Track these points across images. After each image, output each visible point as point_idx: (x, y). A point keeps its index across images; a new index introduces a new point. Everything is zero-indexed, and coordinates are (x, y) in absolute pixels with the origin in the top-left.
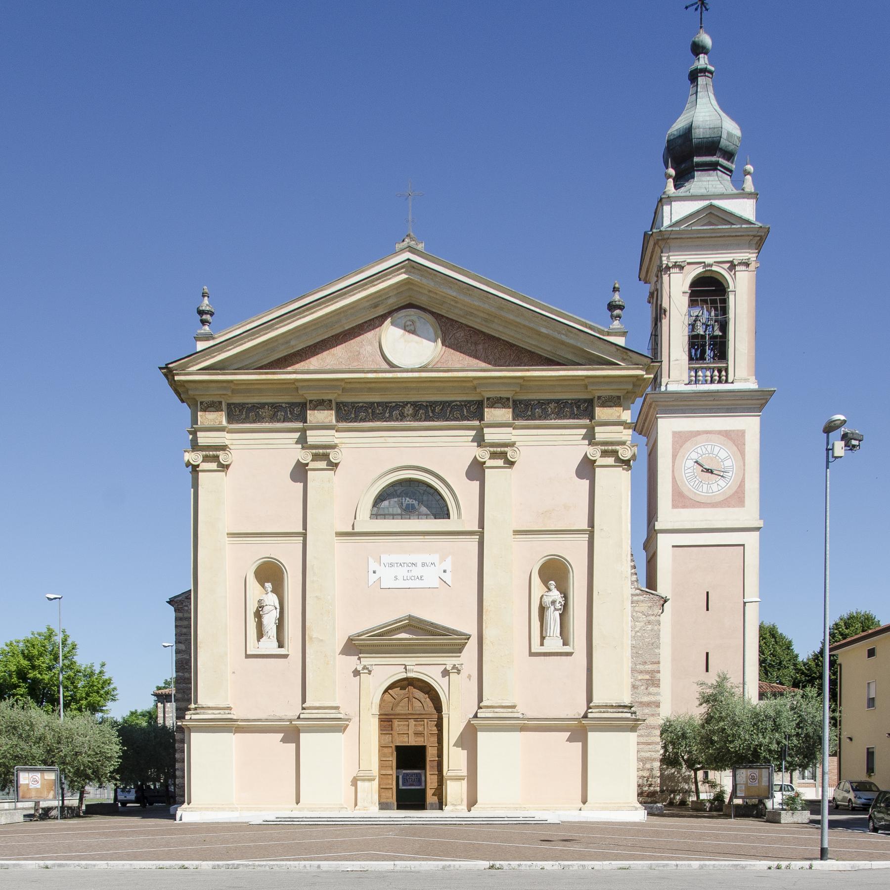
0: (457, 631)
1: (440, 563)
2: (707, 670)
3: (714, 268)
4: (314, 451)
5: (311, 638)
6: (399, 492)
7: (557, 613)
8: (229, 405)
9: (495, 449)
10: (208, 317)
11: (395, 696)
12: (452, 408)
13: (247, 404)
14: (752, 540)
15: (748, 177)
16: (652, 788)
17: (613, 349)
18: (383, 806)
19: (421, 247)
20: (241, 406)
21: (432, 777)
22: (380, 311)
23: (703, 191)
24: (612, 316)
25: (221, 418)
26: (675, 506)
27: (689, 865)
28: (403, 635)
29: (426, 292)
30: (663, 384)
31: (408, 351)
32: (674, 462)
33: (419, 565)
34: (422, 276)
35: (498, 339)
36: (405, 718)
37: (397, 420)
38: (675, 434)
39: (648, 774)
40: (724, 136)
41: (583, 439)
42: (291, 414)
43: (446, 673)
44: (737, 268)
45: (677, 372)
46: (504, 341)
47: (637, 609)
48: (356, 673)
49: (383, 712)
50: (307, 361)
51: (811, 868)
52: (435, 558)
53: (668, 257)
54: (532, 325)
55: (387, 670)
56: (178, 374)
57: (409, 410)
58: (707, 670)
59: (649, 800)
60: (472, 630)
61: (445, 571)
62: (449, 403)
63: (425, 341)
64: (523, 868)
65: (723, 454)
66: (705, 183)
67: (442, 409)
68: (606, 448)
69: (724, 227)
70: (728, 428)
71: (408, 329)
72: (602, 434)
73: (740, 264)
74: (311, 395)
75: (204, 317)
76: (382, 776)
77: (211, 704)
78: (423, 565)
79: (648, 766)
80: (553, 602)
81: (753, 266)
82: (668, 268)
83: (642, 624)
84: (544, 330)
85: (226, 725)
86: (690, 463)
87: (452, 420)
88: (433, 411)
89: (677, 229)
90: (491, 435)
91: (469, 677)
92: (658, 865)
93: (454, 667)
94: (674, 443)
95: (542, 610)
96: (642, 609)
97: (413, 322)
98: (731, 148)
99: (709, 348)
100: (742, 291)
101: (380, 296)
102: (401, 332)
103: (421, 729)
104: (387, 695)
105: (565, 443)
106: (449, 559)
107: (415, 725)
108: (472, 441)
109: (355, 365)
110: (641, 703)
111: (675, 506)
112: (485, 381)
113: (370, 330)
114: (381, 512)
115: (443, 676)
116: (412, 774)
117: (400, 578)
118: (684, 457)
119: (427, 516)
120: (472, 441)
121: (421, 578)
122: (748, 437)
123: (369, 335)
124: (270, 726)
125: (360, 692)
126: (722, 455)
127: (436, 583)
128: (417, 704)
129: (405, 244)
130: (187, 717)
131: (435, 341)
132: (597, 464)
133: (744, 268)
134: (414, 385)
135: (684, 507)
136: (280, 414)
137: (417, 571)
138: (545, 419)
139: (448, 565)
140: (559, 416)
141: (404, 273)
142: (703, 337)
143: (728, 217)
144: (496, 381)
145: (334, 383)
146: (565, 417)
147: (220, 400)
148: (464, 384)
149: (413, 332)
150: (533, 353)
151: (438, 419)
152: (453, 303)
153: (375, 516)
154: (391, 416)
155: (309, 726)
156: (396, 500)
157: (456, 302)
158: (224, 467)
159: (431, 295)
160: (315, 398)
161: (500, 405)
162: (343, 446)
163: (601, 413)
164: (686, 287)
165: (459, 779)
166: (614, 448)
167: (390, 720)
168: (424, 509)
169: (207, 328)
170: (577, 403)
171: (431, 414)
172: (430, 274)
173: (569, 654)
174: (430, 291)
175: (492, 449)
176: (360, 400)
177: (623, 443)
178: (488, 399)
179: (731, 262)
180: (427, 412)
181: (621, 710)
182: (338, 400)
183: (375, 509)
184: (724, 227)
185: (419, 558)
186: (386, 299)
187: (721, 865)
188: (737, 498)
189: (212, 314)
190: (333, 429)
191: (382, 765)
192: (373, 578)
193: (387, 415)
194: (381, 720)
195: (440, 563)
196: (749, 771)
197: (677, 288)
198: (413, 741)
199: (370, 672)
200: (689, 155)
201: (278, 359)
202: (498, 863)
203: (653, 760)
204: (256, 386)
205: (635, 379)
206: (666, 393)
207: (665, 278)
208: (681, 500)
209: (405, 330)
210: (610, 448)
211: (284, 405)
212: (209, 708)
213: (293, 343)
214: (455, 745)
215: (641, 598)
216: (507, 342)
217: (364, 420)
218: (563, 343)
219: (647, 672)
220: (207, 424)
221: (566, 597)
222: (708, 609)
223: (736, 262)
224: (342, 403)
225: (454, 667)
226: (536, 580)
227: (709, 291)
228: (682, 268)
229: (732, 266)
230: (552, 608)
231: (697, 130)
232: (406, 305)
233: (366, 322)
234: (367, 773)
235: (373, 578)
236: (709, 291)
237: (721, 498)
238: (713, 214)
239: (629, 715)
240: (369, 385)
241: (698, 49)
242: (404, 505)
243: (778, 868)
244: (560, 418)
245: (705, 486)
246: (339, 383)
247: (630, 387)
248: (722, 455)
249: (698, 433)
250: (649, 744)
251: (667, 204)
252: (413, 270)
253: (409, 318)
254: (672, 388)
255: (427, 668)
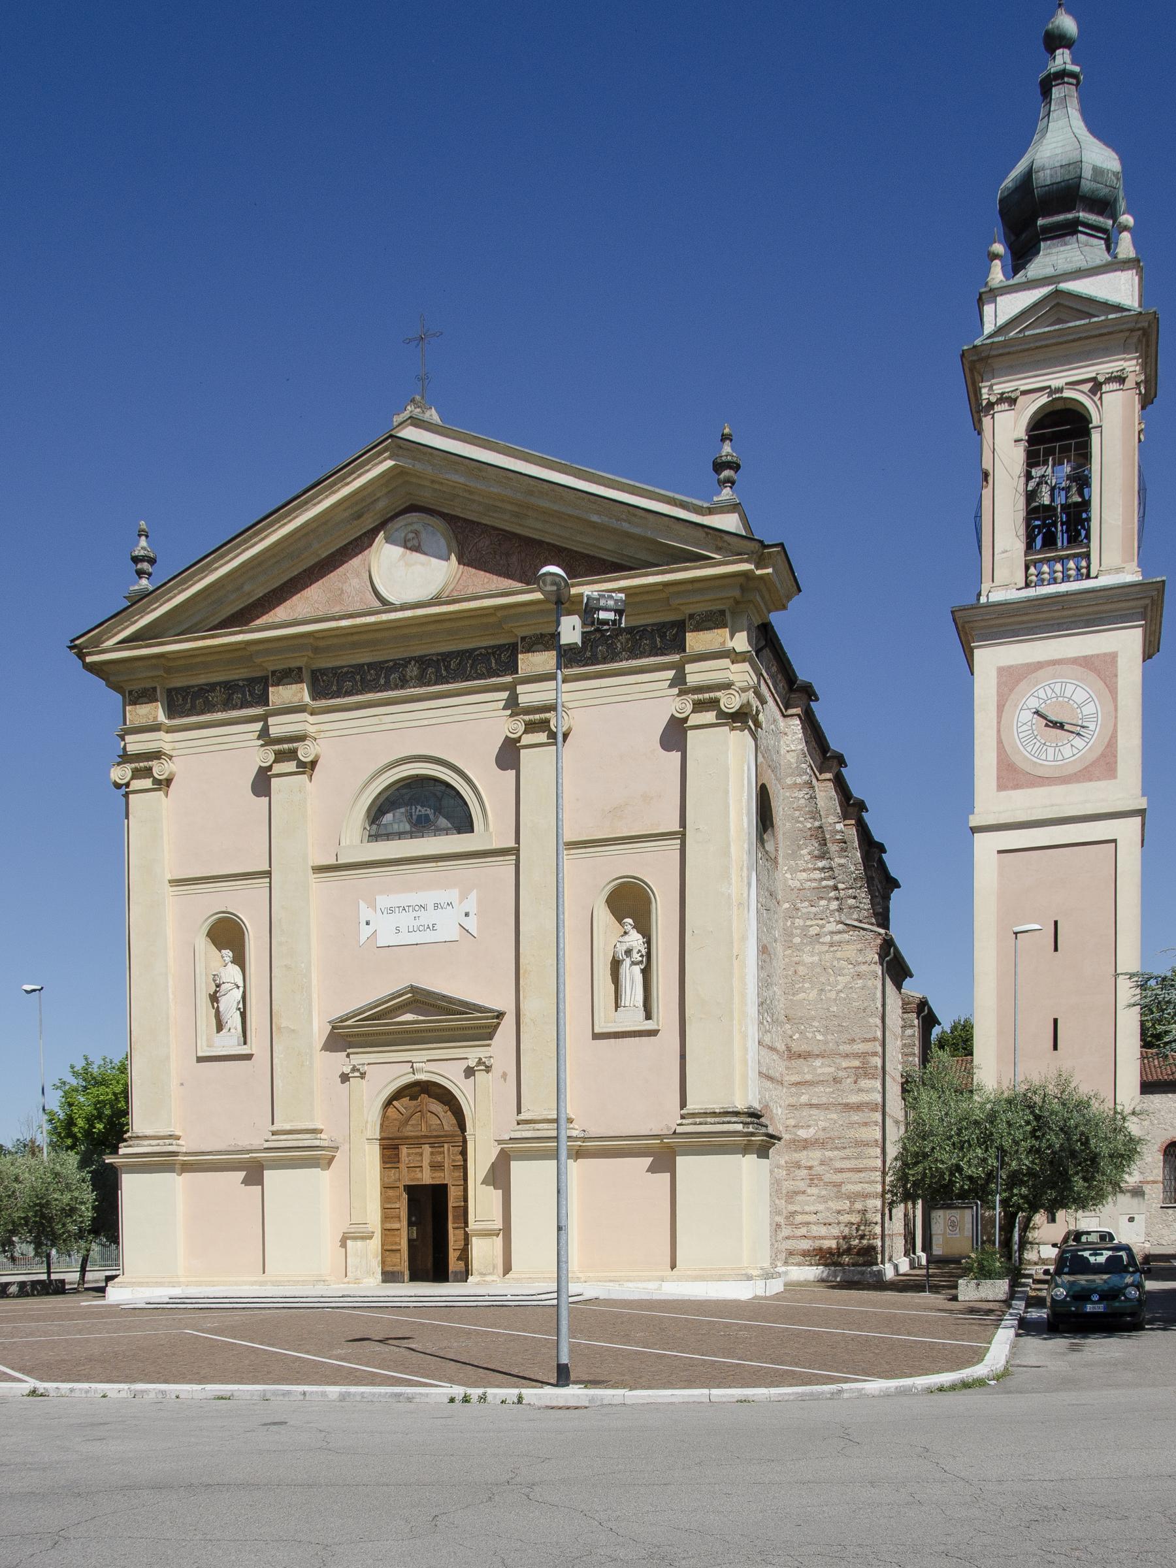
0: (480, 1007)
1: (460, 903)
2: (1055, 1048)
3: (1067, 394)
4: (276, 747)
5: (279, 1028)
6: (407, 797)
7: (637, 970)
8: (169, 691)
9: (531, 717)
10: (145, 566)
11: (403, 1110)
12: (474, 661)
13: (193, 687)
14: (1128, 831)
15: (997, 263)
16: (865, 1242)
17: (700, 534)
18: (389, 1276)
19: (433, 415)
20: (185, 691)
21: (457, 1231)
22: (369, 523)
23: (1049, 271)
24: (719, 481)
25: (158, 712)
26: (1001, 787)
27: (324, 1394)
28: (409, 1017)
29: (428, 484)
30: (984, 593)
31: (407, 577)
32: (999, 717)
33: (430, 907)
34: (414, 459)
35: (540, 543)
36: (416, 1142)
37: (396, 687)
38: (1001, 671)
39: (858, 1220)
40: (1087, 173)
41: (670, 686)
42: (446, 670)
43: (469, 1072)
44: (1105, 388)
45: (1005, 571)
46: (548, 544)
47: (839, 955)
48: (345, 1078)
49: (384, 1135)
50: (271, 613)
51: (520, 1400)
52: (453, 895)
53: (991, 387)
54: (576, 513)
55: (388, 1070)
56: (89, 654)
57: (413, 671)
58: (1055, 1048)
59: (861, 1260)
60: (508, 1006)
61: (467, 915)
62: (469, 653)
63: (434, 561)
64: (77, 1394)
65: (1080, 696)
66: (1053, 258)
67: (459, 664)
68: (700, 696)
69: (1078, 323)
70: (1089, 652)
71: (409, 545)
72: (696, 674)
73: (1109, 380)
74: (273, 664)
75: (139, 566)
76: (386, 1232)
77: (149, 1132)
78: (436, 906)
79: (858, 1206)
80: (628, 952)
81: (1130, 383)
82: (991, 405)
83: (848, 978)
84: (595, 518)
85: (165, 1162)
86: (1027, 716)
87: (475, 679)
88: (447, 668)
89: (1001, 339)
90: (529, 695)
91: (504, 1076)
92: (275, 1393)
93: (480, 1062)
94: (1000, 685)
95: (616, 965)
96: (848, 954)
97: (417, 533)
98: (1104, 191)
99: (1058, 526)
100: (1115, 422)
101: (363, 500)
102: (400, 550)
103: (439, 1159)
104: (391, 1110)
105: (643, 696)
106: (473, 896)
107: (432, 1153)
108: (504, 708)
109: (336, 610)
110: (846, 1105)
111: (1001, 787)
112: (512, 611)
113: (357, 555)
114: (382, 831)
115: (467, 1077)
116: (429, 1232)
117: (404, 929)
118: (1016, 706)
119: (447, 831)
120: (504, 708)
121: (433, 927)
122: (1122, 662)
123: (355, 562)
124: (227, 1161)
125: (346, 1107)
126: (1079, 697)
127: (454, 934)
128: (434, 1121)
129: (406, 414)
130: (121, 1151)
131: (448, 559)
132: (689, 723)
133: (1115, 386)
134: (414, 630)
135: (1017, 787)
136: (237, 697)
137: (427, 918)
138: (612, 660)
139: (471, 904)
140: (634, 654)
141: (390, 458)
142: (1049, 509)
143: (1088, 306)
144: (529, 609)
145: (296, 642)
146: (642, 655)
147: (154, 685)
148: (485, 620)
149: (417, 549)
150: (594, 557)
151: (455, 680)
152: (466, 495)
153: (374, 837)
154: (387, 682)
155: (274, 1160)
156: (403, 810)
157: (471, 493)
158: (164, 784)
159: (436, 486)
160: (279, 667)
161: (540, 647)
162: (322, 735)
163: (696, 641)
164: (1021, 432)
165: (488, 1234)
166: (712, 695)
167: (396, 1148)
168: (443, 822)
169: (144, 582)
170: (661, 628)
171: (444, 673)
172: (425, 454)
173: (653, 1033)
174: (433, 482)
175: (527, 718)
176: (343, 663)
177: (728, 686)
178: (523, 639)
179: (1094, 379)
180: (438, 670)
181: (727, 1119)
182: (314, 667)
183: (374, 827)
184: (1078, 323)
185: (428, 897)
186: (372, 503)
187: (374, 1394)
188: (1104, 765)
189: (152, 561)
190: (303, 711)
191: (387, 1215)
192: (365, 932)
193: (382, 681)
194: (384, 1148)
195: (460, 903)
196: (949, 1213)
197: (1007, 432)
198: (427, 1177)
199: (363, 1076)
200: (1036, 215)
201: (233, 615)
202: (42, 1386)
203: (866, 1196)
204: (199, 660)
205: (742, 580)
206: (989, 605)
207: (986, 421)
208: (1011, 775)
209: (406, 547)
210: (707, 696)
211: (241, 683)
212: (146, 1137)
213: (247, 588)
214: (485, 1182)
215: (846, 936)
216: (554, 545)
217: (349, 693)
218: (629, 535)
219: (856, 1056)
220: (138, 722)
221: (648, 943)
222: (1056, 949)
223: (1101, 379)
224: (319, 670)
225: (480, 1062)
226: (604, 916)
227: (1061, 433)
228: (1013, 401)
229: (1096, 386)
230: (628, 961)
231: (1041, 174)
232: (422, 506)
233: (350, 543)
234: (361, 1228)
235: (365, 932)
236: (1061, 433)
237: (1078, 767)
238: (1062, 305)
239: (739, 1127)
240: (350, 639)
241: (1055, 41)
242: (414, 817)
243: (466, 1399)
244: (636, 657)
245: (1051, 751)
246: (305, 641)
247: (737, 593)
248: (1079, 697)
249: (1040, 666)
250: (860, 1171)
251: (989, 303)
252: (401, 452)
253: (410, 528)
254: (997, 596)
255: (442, 1065)
